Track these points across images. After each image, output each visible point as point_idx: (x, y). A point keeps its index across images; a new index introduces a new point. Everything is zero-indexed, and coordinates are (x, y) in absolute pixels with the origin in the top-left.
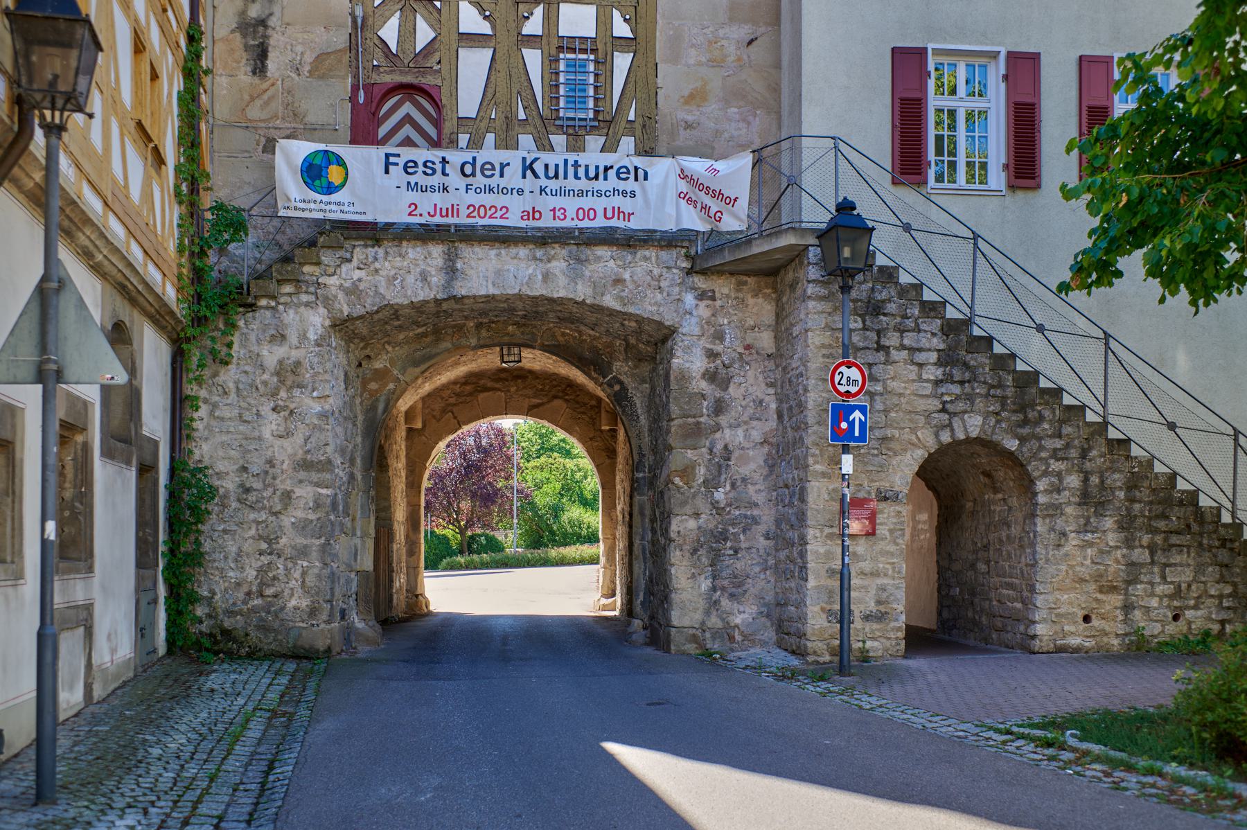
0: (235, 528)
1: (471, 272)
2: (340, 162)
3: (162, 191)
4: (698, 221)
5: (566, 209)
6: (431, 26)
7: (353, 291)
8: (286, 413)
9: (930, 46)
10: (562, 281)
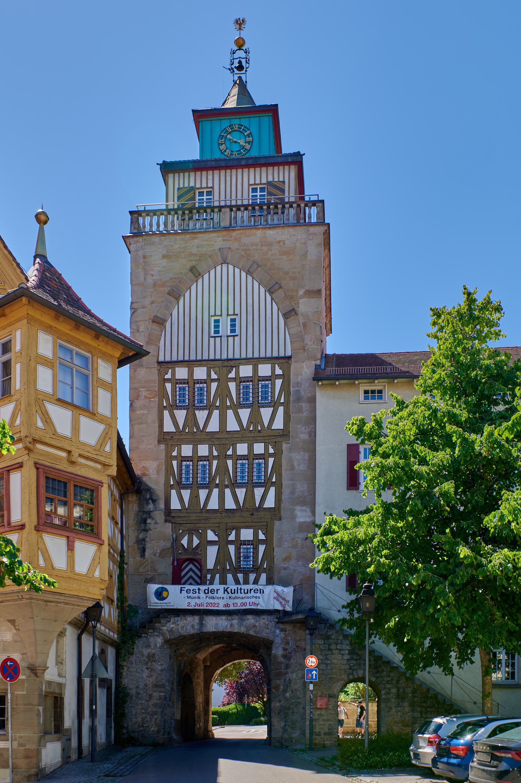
1: (208, 625)
2: (166, 590)
5: (238, 603)
6: (198, 539)
7: (171, 631)
10: (236, 626)
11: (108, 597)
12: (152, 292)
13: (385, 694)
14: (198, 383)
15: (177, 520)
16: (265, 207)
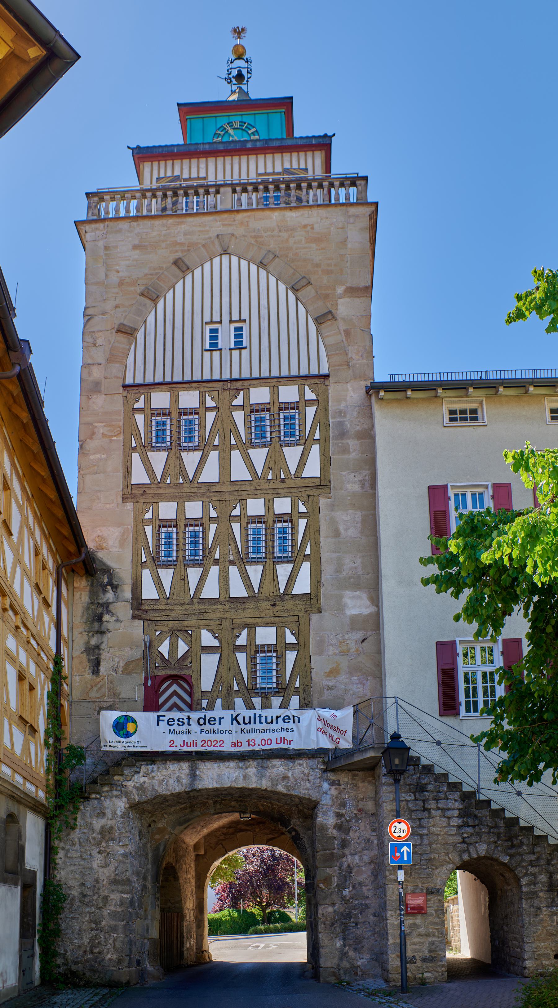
0: (78, 916)
1: (204, 777)
2: (134, 721)
3: (36, 745)
4: (328, 743)
5: (257, 740)
6: (186, 644)
7: (141, 788)
8: (105, 854)
9: (458, 640)
10: (254, 779)
11: (21, 717)
12: (117, 293)
13: (527, 885)
14: (185, 414)
15: (152, 615)
16: (283, 186)
